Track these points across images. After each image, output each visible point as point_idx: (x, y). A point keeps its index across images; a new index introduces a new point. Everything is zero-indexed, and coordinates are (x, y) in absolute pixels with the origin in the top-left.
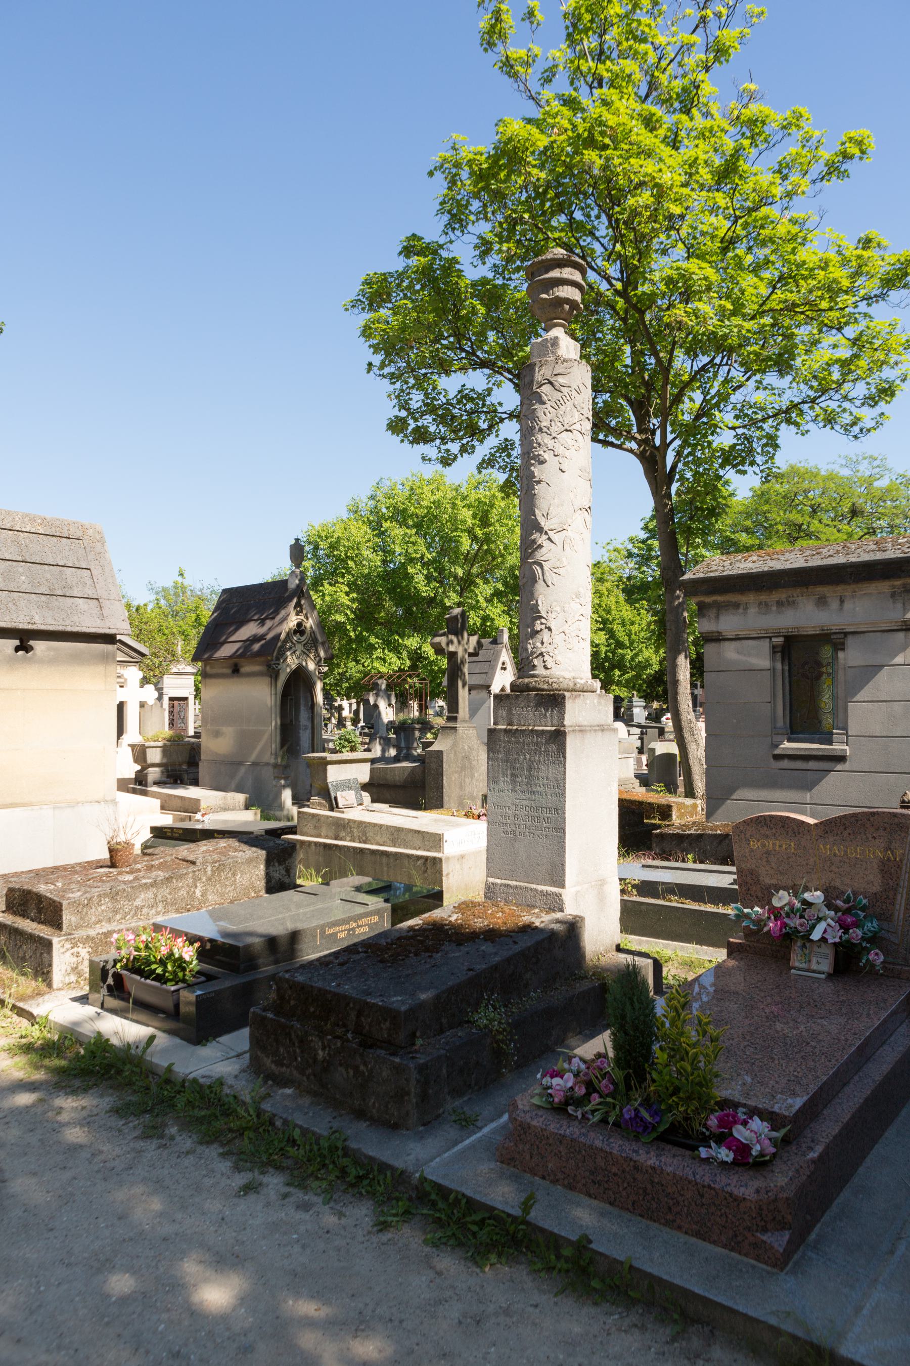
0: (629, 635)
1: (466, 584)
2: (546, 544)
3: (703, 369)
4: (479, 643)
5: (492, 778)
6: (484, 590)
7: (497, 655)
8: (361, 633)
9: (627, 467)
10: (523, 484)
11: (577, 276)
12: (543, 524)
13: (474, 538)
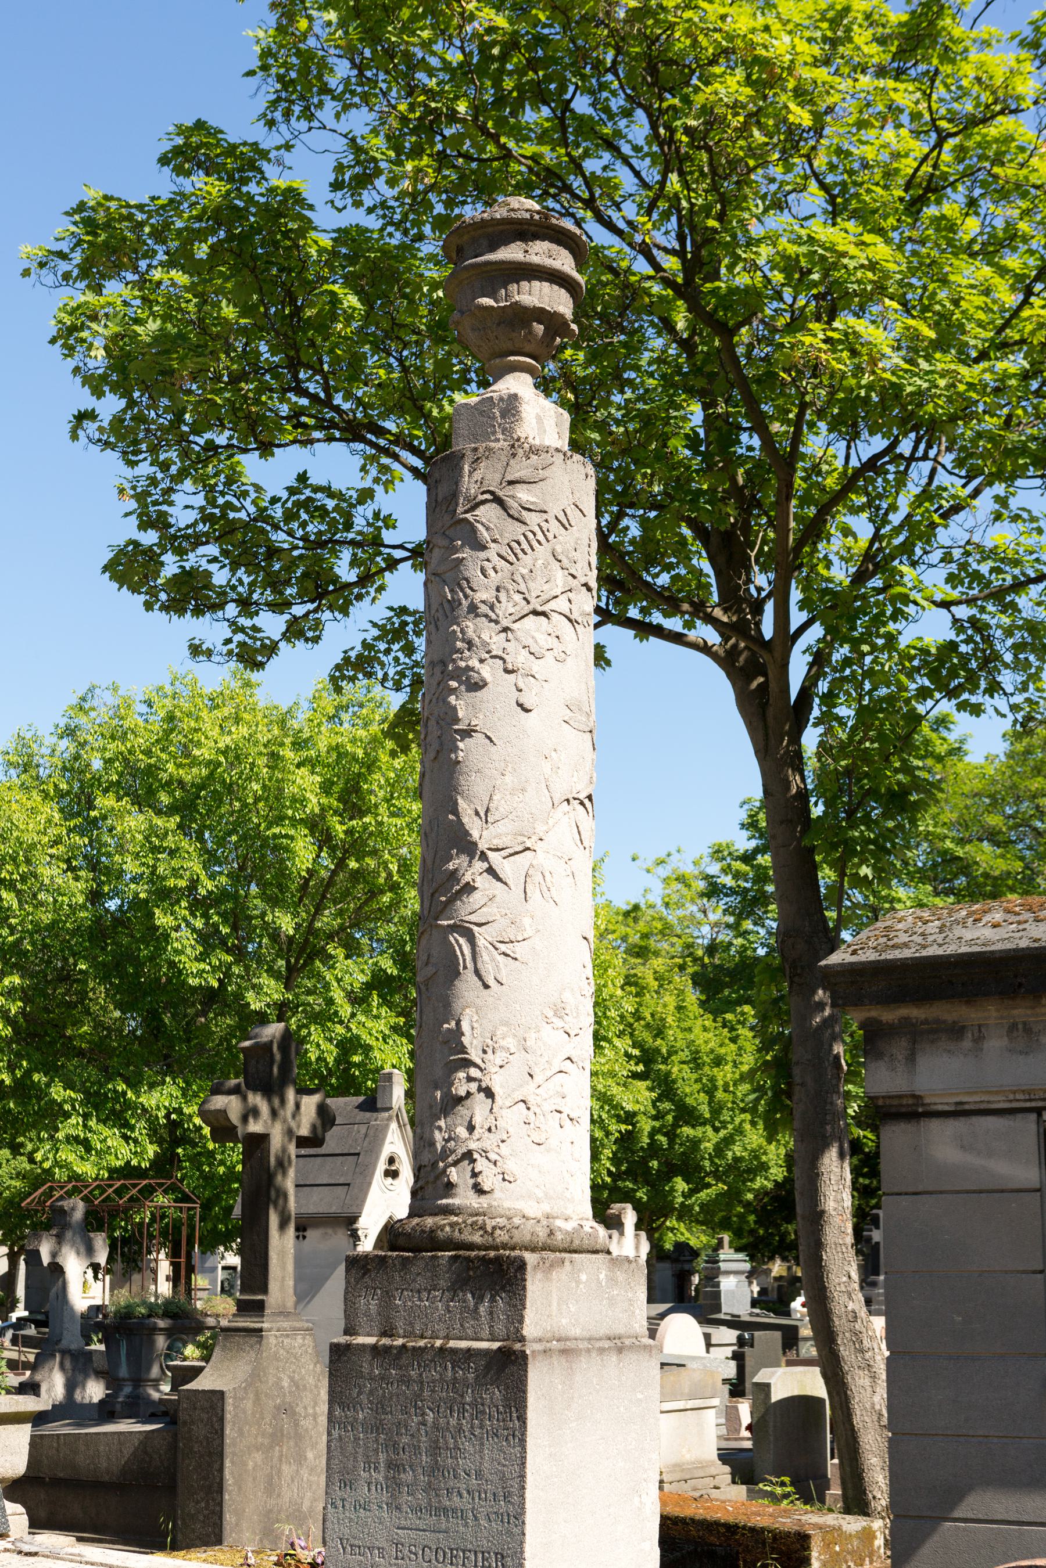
0: (710, 1092)
1: (302, 956)
2: (483, 882)
3: (872, 464)
4: (322, 1110)
5: (340, 1475)
6: (347, 972)
7: (377, 1139)
8: (28, 1073)
9: (689, 691)
10: (431, 729)
11: (564, 261)
12: (475, 834)
13: (325, 840)
